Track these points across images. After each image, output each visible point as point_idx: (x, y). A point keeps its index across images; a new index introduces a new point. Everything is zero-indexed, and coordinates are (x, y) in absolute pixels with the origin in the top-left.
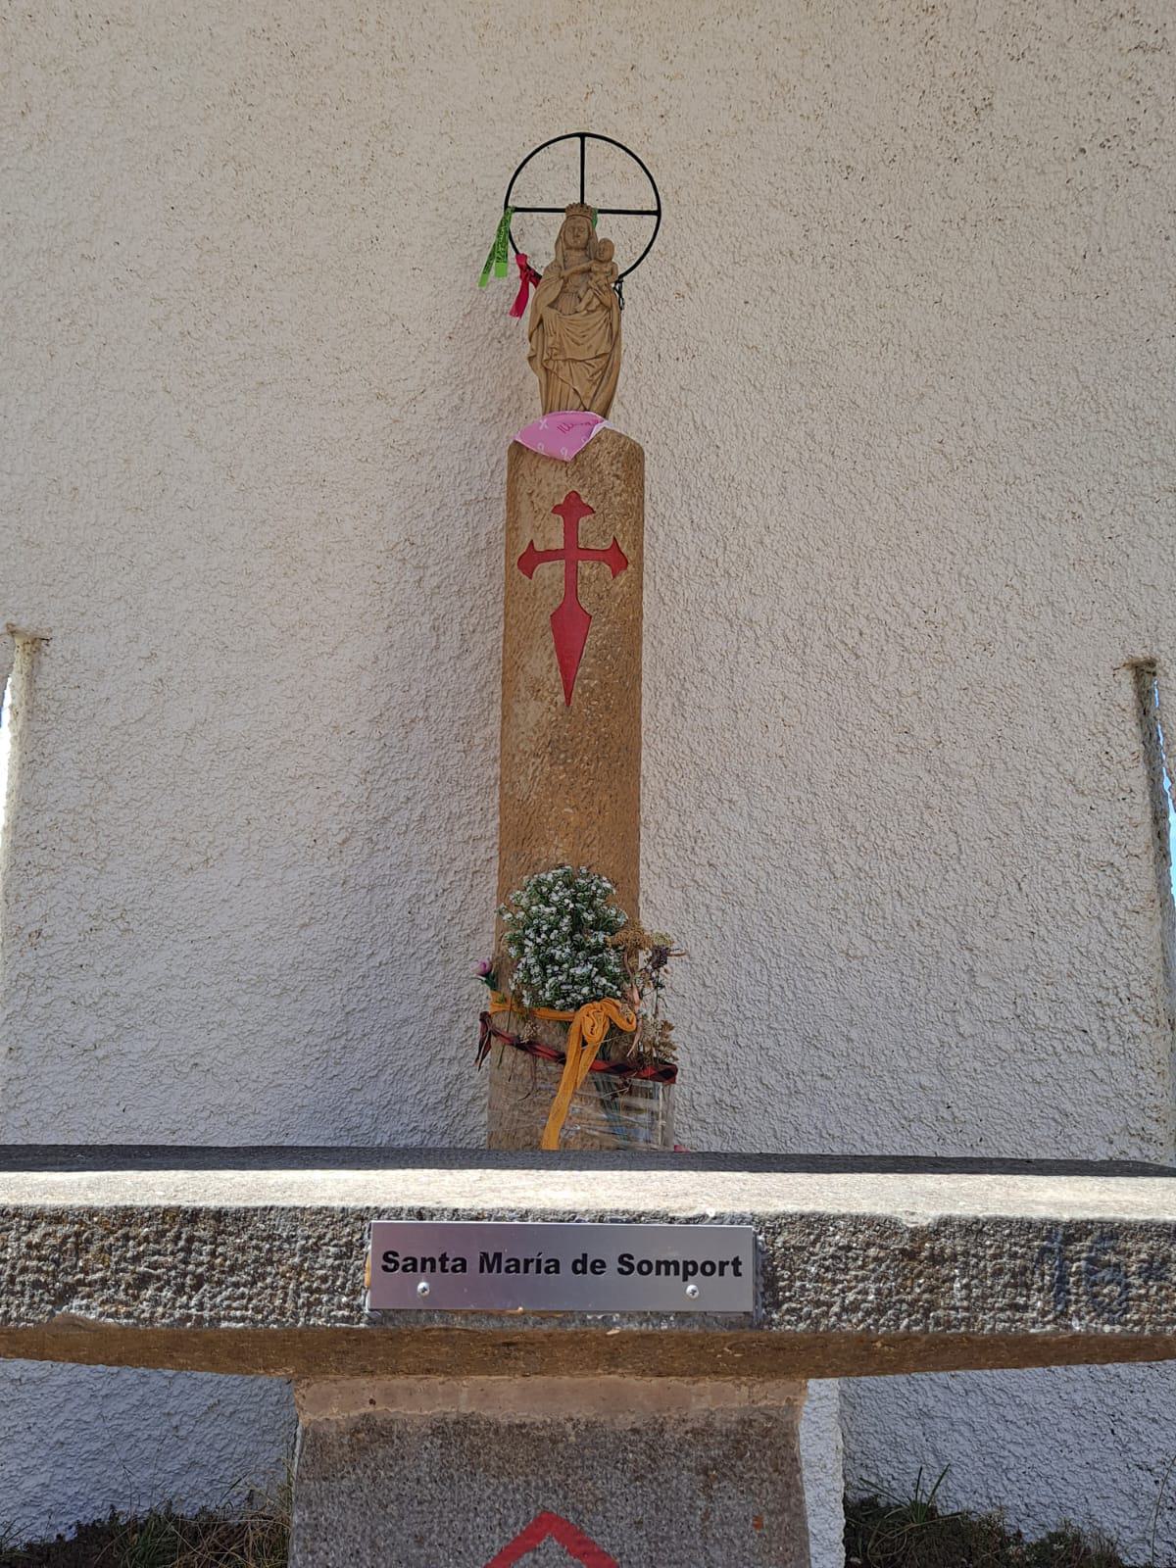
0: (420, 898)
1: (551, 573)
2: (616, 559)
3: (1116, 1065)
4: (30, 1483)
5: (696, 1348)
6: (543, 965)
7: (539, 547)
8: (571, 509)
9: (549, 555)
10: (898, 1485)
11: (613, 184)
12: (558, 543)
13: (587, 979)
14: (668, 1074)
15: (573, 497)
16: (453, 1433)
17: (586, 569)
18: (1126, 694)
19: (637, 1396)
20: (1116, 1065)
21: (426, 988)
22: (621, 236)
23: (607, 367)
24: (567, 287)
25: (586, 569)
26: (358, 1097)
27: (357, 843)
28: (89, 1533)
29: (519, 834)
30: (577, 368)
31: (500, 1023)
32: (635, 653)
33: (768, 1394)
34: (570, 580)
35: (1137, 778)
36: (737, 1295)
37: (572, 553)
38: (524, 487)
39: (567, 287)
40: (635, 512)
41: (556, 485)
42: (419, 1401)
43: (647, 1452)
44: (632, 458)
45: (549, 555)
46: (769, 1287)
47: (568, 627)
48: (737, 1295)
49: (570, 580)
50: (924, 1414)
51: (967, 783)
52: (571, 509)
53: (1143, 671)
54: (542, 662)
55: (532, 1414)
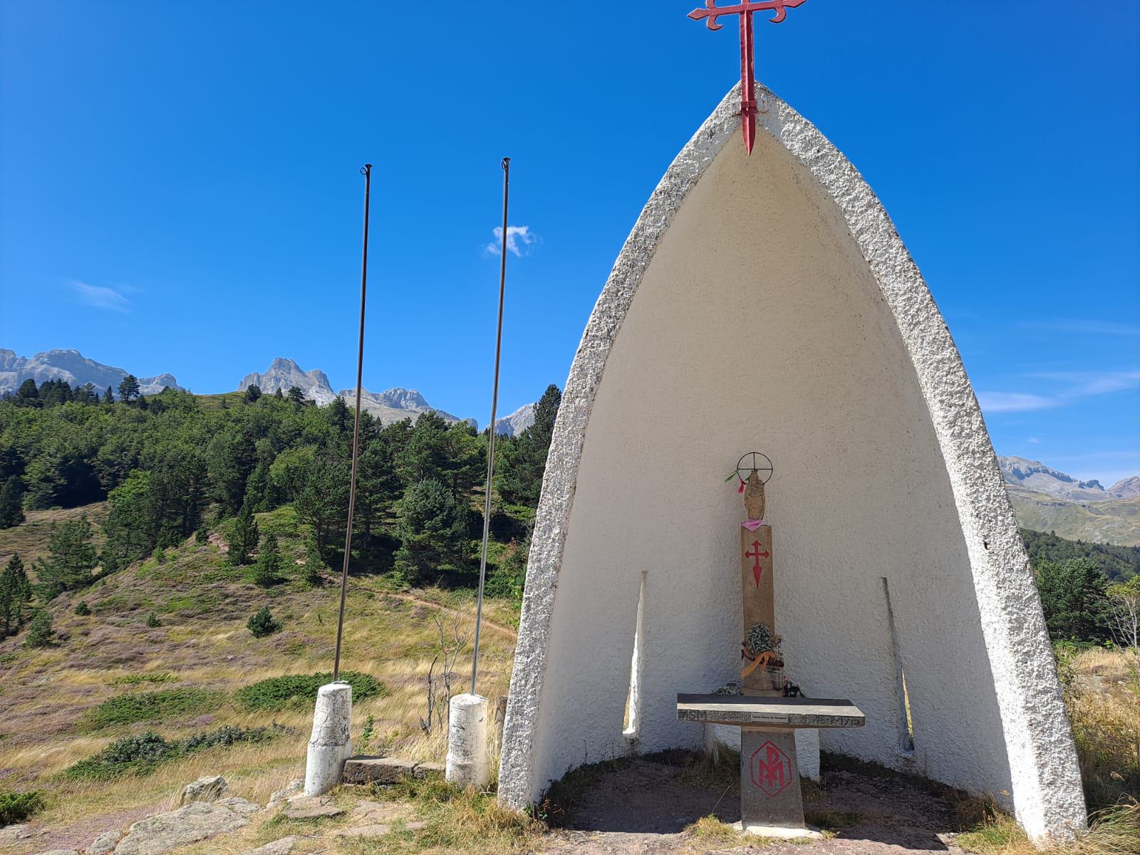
0: (723, 619)
1: (752, 558)
2: (766, 554)
3: (882, 663)
4: (654, 741)
5: (782, 725)
6: (755, 644)
7: (750, 552)
8: (756, 544)
9: (752, 554)
10: (835, 748)
11: (761, 462)
12: (754, 557)
13: (765, 648)
14: (782, 665)
15: (756, 541)
16: (758, 732)
17: (760, 557)
18: (881, 584)
19: (778, 730)
20: (882, 663)
21: (727, 639)
22: (762, 476)
23: (762, 509)
24: (752, 487)
25: (760, 557)
26: (713, 663)
27: (709, 607)
28: (665, 751)
29: (748, 615)
30: (756, 509)
31: (746, 653)
32: (772, 573)
33: (791, 730)
34: (755, 557)
35: (884, 602)
36: (786, 721)
37: (757, 554)
38: (745, 537)
39: (752, 487)
40: (770, 543)
41: (753, 539)
42: (755, 729)
43: (779, 735)
44: (769, 530)
45: (752, 554)
46: (789, 720)
47: (757, 570)
48: (786, 721)
49: (755, 557)
50: (843, 735)
51: (848, 599)
52: (756, 544)
53: (885, 580)
54: (752, 578)
55: (766, 731)
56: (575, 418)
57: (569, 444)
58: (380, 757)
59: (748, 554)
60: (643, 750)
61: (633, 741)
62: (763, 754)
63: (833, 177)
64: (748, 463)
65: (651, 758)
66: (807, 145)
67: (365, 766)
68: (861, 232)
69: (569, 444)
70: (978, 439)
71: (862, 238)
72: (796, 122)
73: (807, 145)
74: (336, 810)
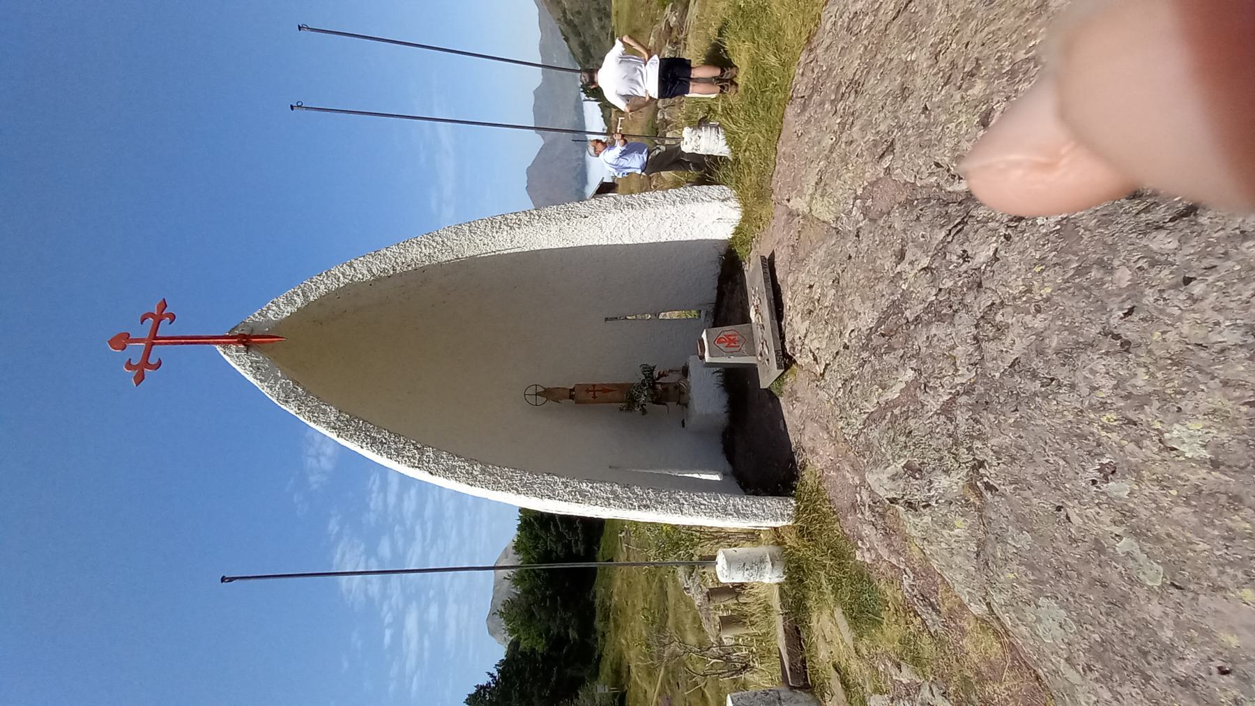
2: (594, 386)
11: (532, 391)
39: (548, 393)
56: (490, 475)
57: (511, 478)
58: (781, 657)
59: (594, 397)
60: (729, 468)
61: (724, 475)
62: (721, 346)
63: (322, 287)
64: (532, 400)
65: (731, 460)
66: (290, 302)
67: (791, 664)
68: (370, 271)
69: (511, 478)
70: (522, 216)
71: (375, 271)
72: (269, 308)
73: (290, 302)
74: (834, 674)
